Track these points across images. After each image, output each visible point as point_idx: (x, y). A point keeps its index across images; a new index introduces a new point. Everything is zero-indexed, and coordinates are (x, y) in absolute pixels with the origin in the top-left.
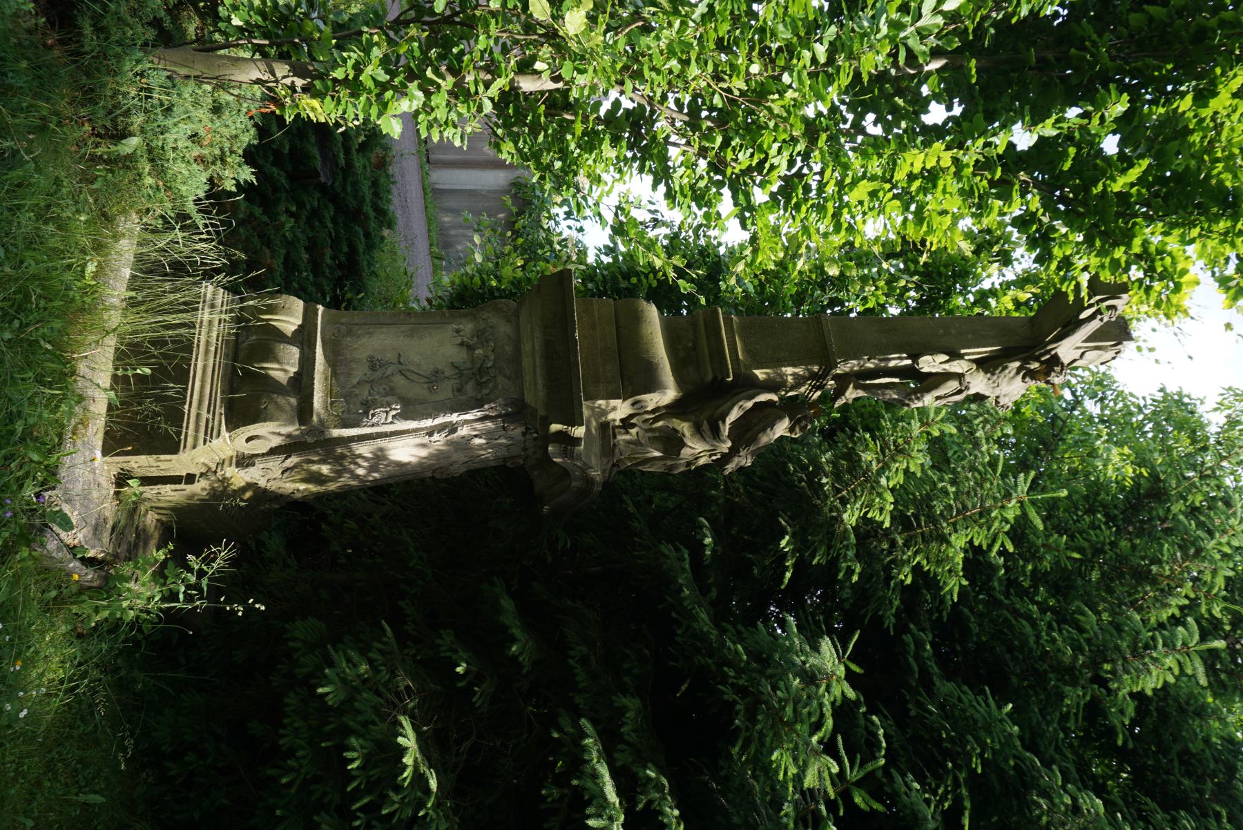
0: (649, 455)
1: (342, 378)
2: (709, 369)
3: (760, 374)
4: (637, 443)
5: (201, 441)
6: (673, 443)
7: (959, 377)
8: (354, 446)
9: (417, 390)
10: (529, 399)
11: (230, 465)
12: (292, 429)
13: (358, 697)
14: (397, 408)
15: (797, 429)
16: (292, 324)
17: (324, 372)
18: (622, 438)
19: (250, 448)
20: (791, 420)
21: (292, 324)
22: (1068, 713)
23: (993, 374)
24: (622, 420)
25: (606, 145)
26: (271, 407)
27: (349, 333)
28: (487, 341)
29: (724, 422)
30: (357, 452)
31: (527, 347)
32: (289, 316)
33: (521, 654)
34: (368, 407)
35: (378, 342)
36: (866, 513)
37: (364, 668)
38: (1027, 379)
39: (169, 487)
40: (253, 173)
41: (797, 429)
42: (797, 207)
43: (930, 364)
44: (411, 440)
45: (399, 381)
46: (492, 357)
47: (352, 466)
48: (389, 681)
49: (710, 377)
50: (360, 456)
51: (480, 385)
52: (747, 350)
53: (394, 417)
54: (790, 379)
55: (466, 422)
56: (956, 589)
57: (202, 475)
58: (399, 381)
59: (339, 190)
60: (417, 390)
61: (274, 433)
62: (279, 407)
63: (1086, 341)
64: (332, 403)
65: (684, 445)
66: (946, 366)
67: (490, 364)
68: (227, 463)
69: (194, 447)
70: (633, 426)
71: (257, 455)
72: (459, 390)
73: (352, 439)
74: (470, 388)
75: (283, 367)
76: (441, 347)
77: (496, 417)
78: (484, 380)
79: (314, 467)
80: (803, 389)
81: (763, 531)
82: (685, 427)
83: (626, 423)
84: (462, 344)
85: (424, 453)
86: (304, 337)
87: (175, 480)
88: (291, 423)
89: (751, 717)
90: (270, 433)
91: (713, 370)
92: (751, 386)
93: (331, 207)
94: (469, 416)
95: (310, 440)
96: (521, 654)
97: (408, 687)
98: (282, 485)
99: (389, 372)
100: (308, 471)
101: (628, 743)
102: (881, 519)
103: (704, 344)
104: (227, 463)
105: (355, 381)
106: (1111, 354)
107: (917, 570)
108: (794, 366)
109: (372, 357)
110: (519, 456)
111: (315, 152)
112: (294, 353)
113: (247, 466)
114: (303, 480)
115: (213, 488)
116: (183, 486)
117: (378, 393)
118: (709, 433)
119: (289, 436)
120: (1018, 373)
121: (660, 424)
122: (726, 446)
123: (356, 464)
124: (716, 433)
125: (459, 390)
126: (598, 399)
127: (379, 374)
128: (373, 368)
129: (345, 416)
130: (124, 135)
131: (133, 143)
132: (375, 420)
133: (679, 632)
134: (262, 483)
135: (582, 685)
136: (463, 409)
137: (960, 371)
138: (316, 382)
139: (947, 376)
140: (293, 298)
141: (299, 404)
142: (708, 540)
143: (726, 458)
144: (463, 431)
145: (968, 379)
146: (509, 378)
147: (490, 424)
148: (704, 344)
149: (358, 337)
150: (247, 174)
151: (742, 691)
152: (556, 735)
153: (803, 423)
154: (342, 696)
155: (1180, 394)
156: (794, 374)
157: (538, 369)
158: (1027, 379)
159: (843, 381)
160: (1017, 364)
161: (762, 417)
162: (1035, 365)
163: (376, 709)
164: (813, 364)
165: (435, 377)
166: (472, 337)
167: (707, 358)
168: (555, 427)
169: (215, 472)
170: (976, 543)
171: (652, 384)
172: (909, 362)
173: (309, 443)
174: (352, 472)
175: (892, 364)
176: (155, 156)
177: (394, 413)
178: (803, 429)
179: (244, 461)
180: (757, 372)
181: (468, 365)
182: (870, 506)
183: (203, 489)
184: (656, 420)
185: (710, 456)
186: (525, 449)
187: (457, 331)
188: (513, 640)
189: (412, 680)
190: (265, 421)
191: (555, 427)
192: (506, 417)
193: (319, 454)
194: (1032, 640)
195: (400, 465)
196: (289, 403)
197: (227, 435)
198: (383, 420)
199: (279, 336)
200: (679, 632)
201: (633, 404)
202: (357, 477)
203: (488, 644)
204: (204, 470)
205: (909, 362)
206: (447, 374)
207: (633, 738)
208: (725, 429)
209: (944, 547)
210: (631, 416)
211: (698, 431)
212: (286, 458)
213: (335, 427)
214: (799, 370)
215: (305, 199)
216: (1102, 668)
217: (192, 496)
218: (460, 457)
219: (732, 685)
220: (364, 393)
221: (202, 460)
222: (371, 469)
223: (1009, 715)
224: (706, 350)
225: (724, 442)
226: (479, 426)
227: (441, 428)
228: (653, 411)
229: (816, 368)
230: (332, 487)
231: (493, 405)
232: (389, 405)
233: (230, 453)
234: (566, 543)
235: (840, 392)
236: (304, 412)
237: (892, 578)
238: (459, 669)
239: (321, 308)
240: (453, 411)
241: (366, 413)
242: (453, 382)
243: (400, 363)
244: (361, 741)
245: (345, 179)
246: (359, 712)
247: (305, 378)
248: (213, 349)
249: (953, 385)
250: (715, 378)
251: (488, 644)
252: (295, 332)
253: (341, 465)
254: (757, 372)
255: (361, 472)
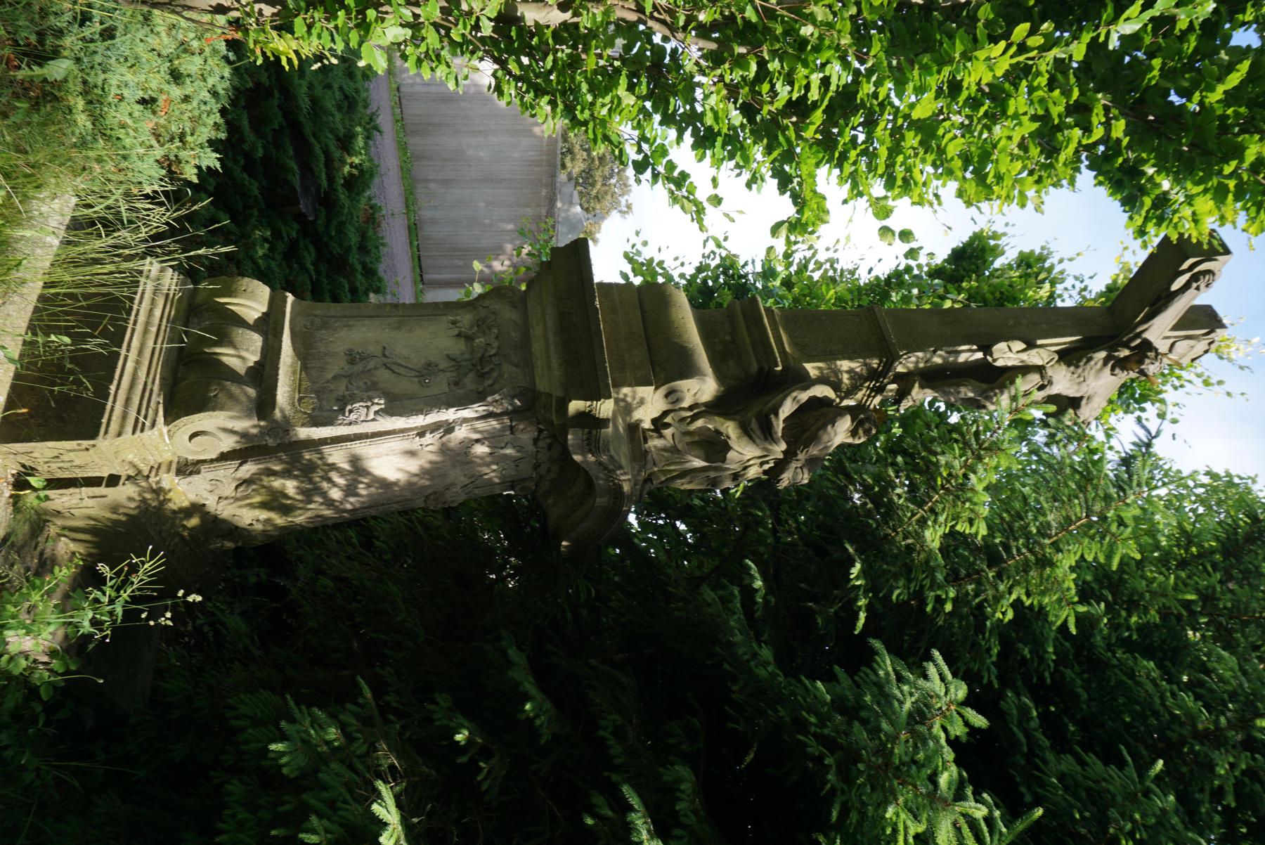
0: (688, 466)
1: (314, 373)
2: (753, 358)
3: (812, 369)
4: (673, 450)
5: (129, 428)
6: (715, 447)
7: (1040, 369)
8: (326, 449)
9: (406, 385)
10: (541, 385)
11: (169, 471)
12: (247, 424)
13: (323, 768)
14: (380, 403)
15: (861, 432)
16: (254, 309)
17: (292, 365)
18: (655, 443)
19: (193, 451)
20: (853, 421)
21: (254, 309)
22: (1221, 788)
23: (1077, 367)
24: (654, 421)
25: (621, 90)
26: (222, 397)
27: (324, 325)
28: (489, 329)
29: (777, 415)
30: (331, 460)
31: (537, 331)
32: (252, 301)
33: (537, 716)
34: (344, 403)
35: (356, 335)
36: (952, 527)
37: (333, 733)
38: (1117, 371)
39: (86, 491)
40: (218, 159)
41: (861, 432)
42: (843, 157)
43: (1007, 354)
44: (396, 444)
45: (383, 375)
46: (495, 344)
47: (325, 485)
48: (367, 754)
49: (755, 367)
50: (333, 467)
51: (482, 376)
52: (794, 343)
53: (376, 413)
54: (845, 377)
55: (465, 420)
56: (1072, 621)
57: (129, 478)
58: (383, 375)
59: (321, 229)
60: (406, 385)
61: (225, 430)
62: (231, 396)
63: (1174, 328)
64: (300, 399)
65: (728, 448)
66: (1024, 356)
67: (493, 352)
68: (164, 468)
69: (119, 435)
70: (668, 426)
71: (204, 461)
72: (456, 384)
73: (324, 442)
74: (469, 382)
75: (242, 353)
76: (436, 342)
77: (502, 414)
78: (486, 369)
79: (277, 483)
80: (859, 395)
81: (826, 574)
82: (730, 429)
83: (659, 424)
84: (459, 335)
85: (413, 466)
86: (268, 326)
87: (94, 482)
88: (249, 416)
89: (846, 775)
90: (219, 427)
91: (758, 361)
92: (806, 382)
93: (312, 249)
94: (467, 413)
95: (271, 442)
96: (537, 716)
97: (392, 767)
98: (238, 512)
99: (371, 365)
100: (271, 491)
101: (684, 827)
102: (973, 530)
103: (744, 332)
104: (164, 468)
105: (330, 376)
106: (1203, 345)
107: (1017, 605)
108: (851, 359)
109: (350, 350)
110: (530, 478)
111: (293, 165)
112: (256, 340)
113: (190, 474)
114: (264, 506)
115: (144, 500)
116: (101, 490)
117: (358, 388)
118: (758, 432)
119: (244, 435)
120: (1105, 364)
121: (700, 423)
122: (780, 448)
123: (329, 480)
124: (767, 433)
125: (456, 384)
126: (624, 385)
127: (358, 367)
128: (352, 361)
129: (317, 413)
130: (56, 54)
131: (59, 69)
132: (353, 417)
133: (734, 688)
134: (211, 504)
135: (619, 761)
136: (462, 403)
137: (1040, 363)
138: (281, 372)
139: (1025, 370)
140: (256, 282)
141: (259, 396)
142: (758, 584)
143: (781, 466)
144: (461, 433)
145: (1050, 372)
146: (517, 366)
147: (494, 423)
148: (744, 332)
149: (335, 330)
150: (211, 159)
151: (830, 744)
152: (589, 821)
153: (867, 426)
154: (302, 761)
155: (1228, 475)
156: (851, 371)
157: (552, 348)
158: (1117, 371)
159: (905, 382)
160: (1103, 354)
161: (815, 416)
162: (1125, 353)
163: (348, 786)
164: (872, 357)
165: (427, 370)
166: (472, 327)
167: (750, 348)
168: (575, 406)
169: (148, 477)
170: (1090, 558)
171: (687, 369)
172: (980, 355)
173: (270, 446)
174: (324, 494)
175: (962, 358)
176: (94, 98)
177: (376, 408)
178: (867, 432)
179: (187, 469)
180: (808, 366)
181: (467, 356)
182: (956, 518)
183: (130, 499)
184: (694, 418)
185: (762, 464)
186: (536, 467)
187: (454, 323)
188: (526, 698)
189: (398, 758)
190: (214, 409)
191: (575, 406)
192: (514, 414)
193: (283, 462)
194: (1157, 701)
195: (384, 484)
196: (246, 394)
197: (165, 429)
198: (365, 417)
199: (240, 322)
200: (734, 688)
201: (667, 396)
202: (330, 503)
203: (495, 712)
204: (132, 472)
205: (980, 355)
206: (441, 367)
207: (692, 820)
208: (779, 426)
209: (1048, 570)
210: (665, 413)
211: (746, 431)
212: (241, 465)
213: (303, 425)
214: (856, 365)
215: (283, 228)
216: (1254, 727)
217: (114, 508)
218: (458, 477)
219: (815, 735)
220: (341, 388)
221: (130, 457)
222: (350, 490)
223: (1158, 779)
224: (748, 340)
225: (775, 442)
226: (481, 425)
227: (435, 427)
228: (691, 408)
229: (875, 363)
230: (300, 518)
231: (497, 397)
232: (370, 399)
233: (168, 456)
234: (589, 592)
235: (902, 394)
236: (264, 405)
237: (987, 618)
238: (459, 737)
239: (290, 298)
240: (449, 405)
241: (342, 411)
242: (449, 374)
243: (385, 356)
244: (325, 822)
245: (329, 220)
246: (325, 788)
247: (267, 368)
248: (154, 329)
249: (1035, 378)
250: (761, 369)
251: (495, 712)
252: (256, 320)
253: (311, 481)
254: (808, 366)
255: (336, 494)
